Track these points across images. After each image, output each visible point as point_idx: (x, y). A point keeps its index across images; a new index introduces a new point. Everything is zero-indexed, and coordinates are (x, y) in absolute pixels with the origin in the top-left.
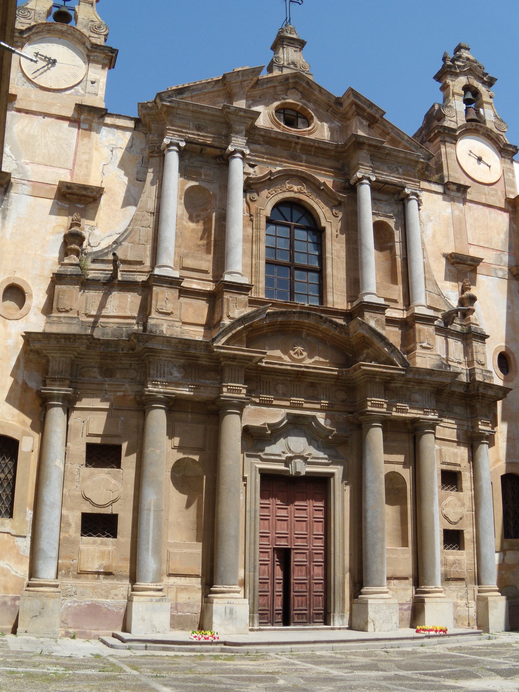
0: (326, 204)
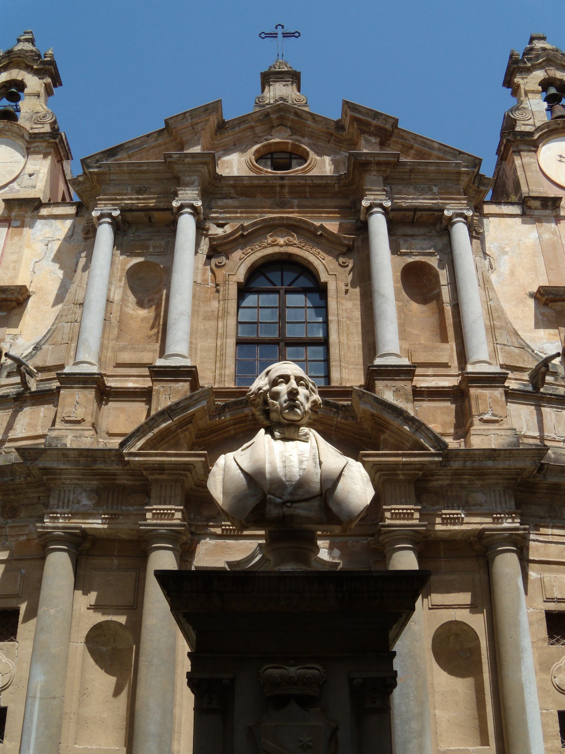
0: (329, 253)
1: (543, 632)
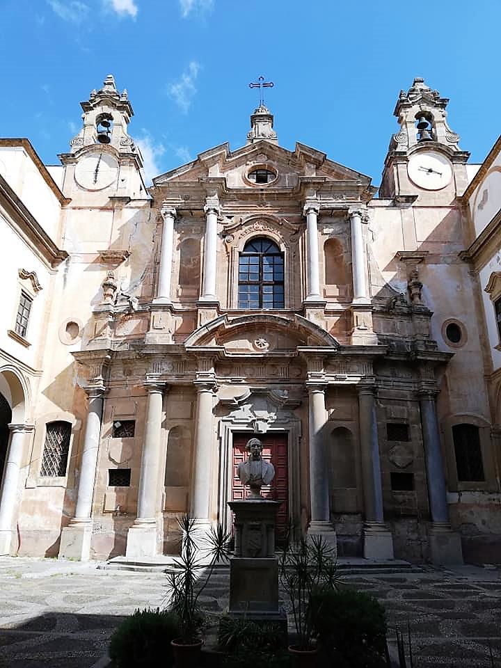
1: (385, 434)
